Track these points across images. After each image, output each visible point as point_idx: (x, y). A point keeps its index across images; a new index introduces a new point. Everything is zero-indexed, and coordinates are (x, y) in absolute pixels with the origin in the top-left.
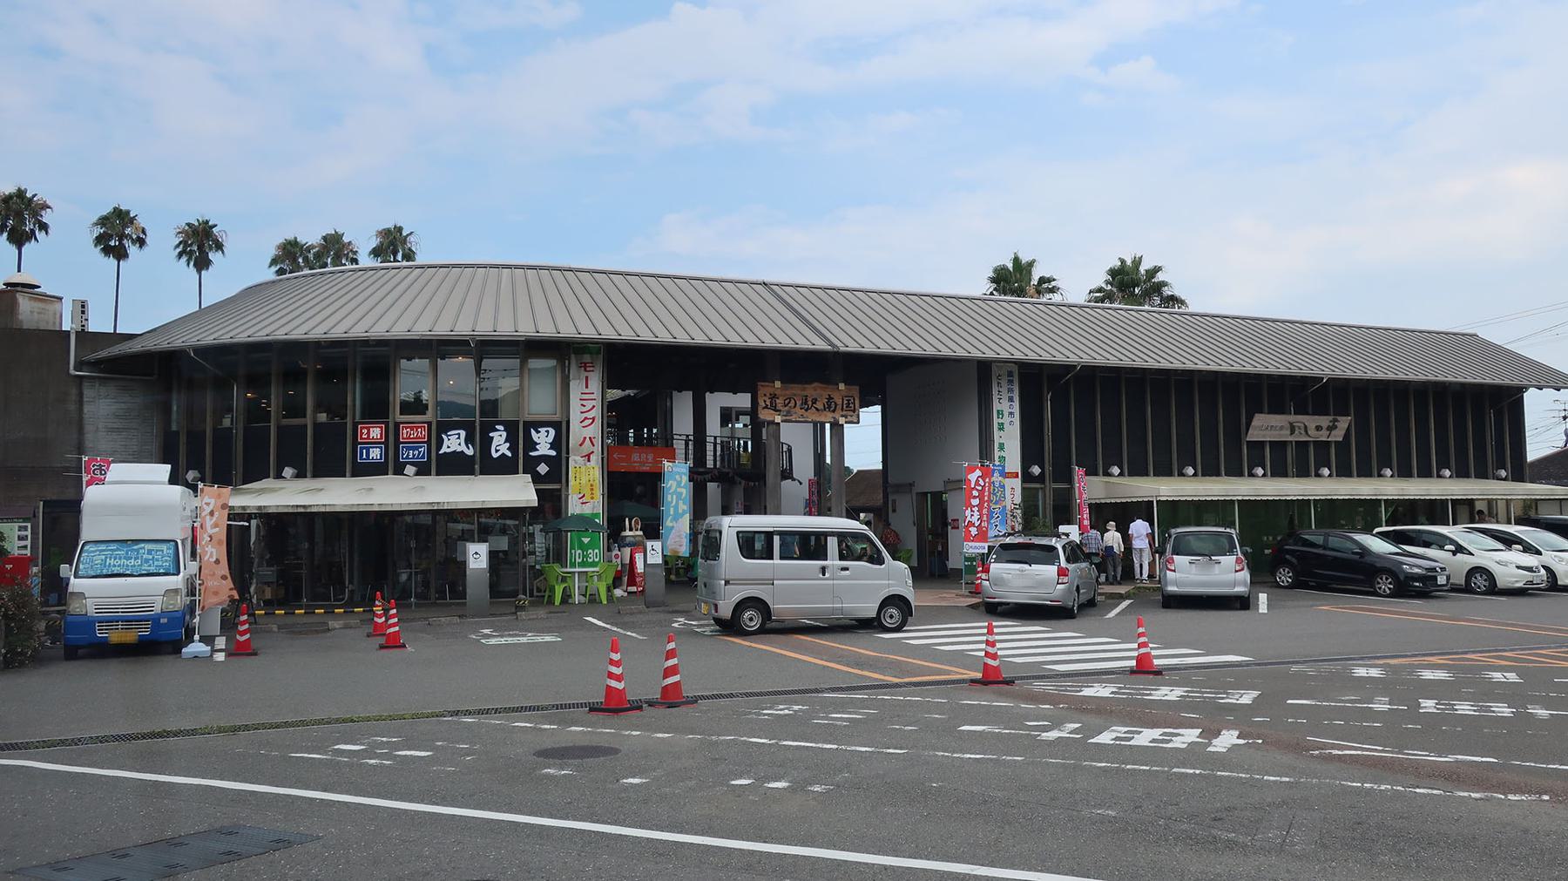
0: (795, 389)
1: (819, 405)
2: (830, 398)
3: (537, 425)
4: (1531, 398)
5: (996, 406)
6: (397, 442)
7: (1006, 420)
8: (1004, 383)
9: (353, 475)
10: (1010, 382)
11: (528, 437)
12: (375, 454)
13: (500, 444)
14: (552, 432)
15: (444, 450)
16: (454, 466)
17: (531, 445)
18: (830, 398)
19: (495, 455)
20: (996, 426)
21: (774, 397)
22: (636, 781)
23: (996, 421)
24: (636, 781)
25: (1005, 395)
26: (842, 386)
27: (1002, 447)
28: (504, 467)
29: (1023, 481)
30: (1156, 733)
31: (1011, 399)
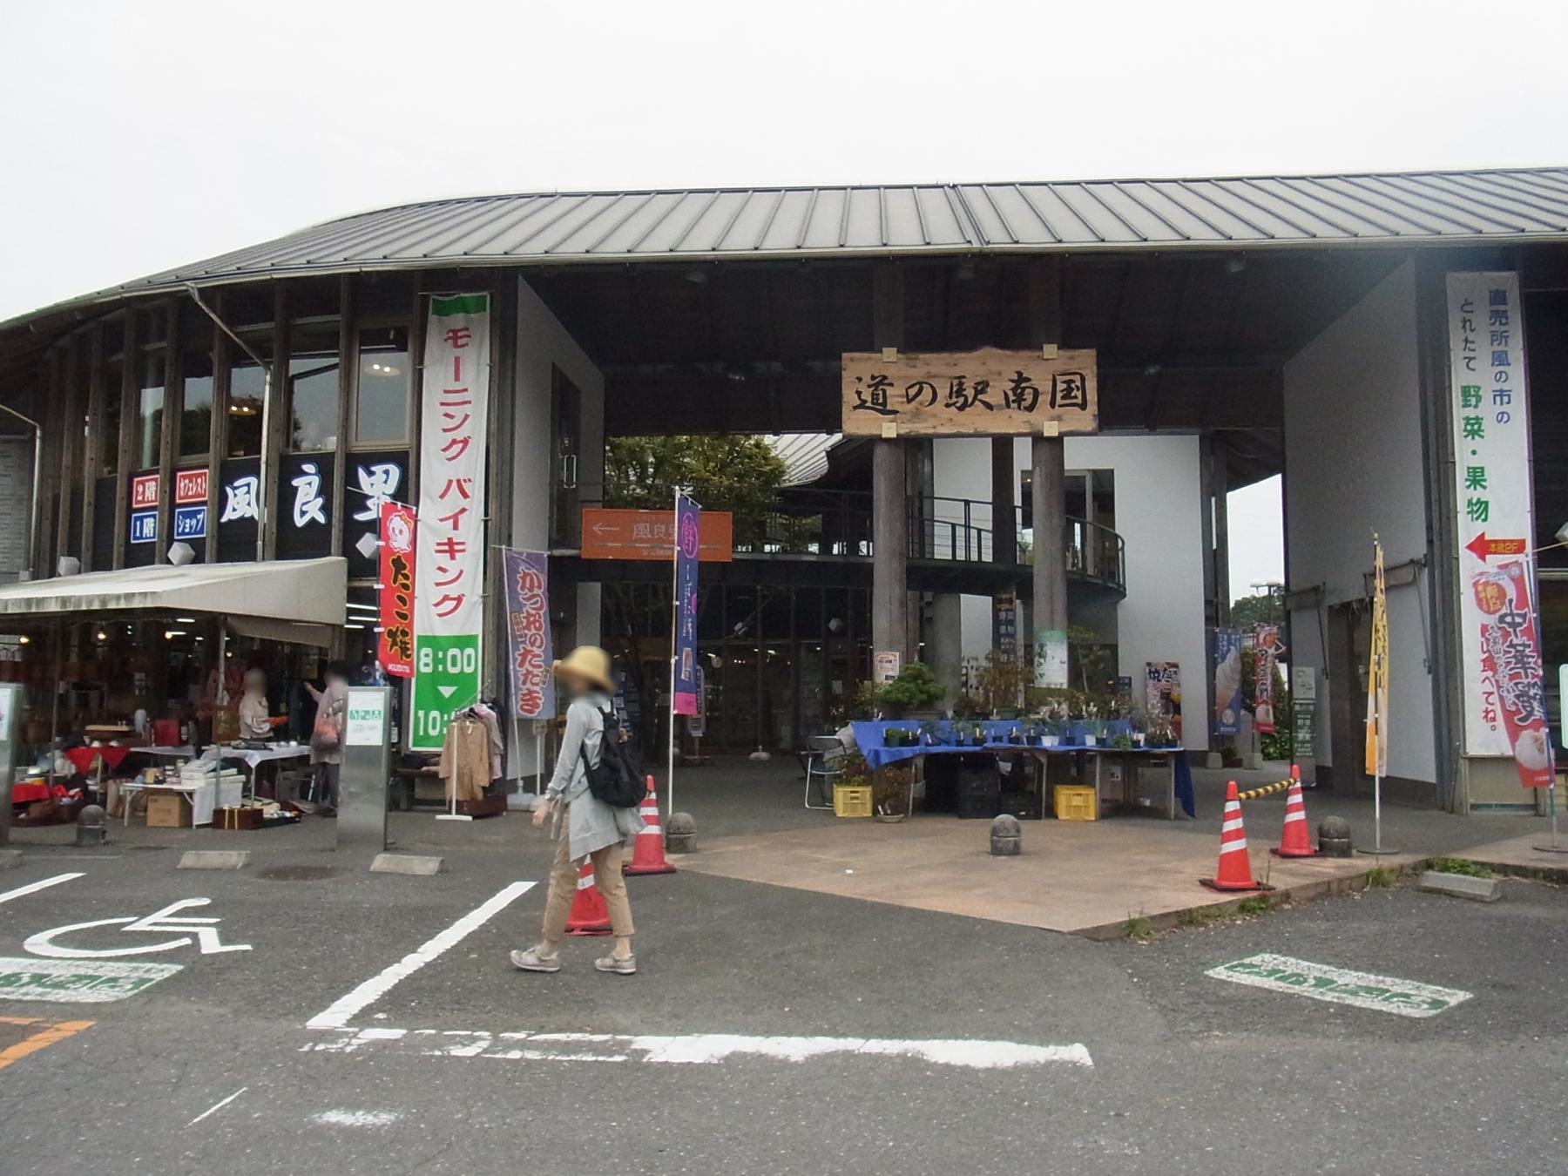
0: (938, 366)
1: (994, 396)
2: (1021, 379)
3: (370, 460)
4: (405, 357)
5: (1460, 377)
6: (173, 505)
7: (1487, 410)
8: (1481, 319)
9: (127, 565)
10: (1499, 316)
11: (351, 479)
12: (149, 528)
13: (308, 504)
14: (395, 471)
15: (224, 520)
16: (234, 543)
17: (357, 501)
18: (1021, 379)
19: (300, 522)
20: (1458, 426)
21: (880, 382)
22: (360, 1118)
23: (1459, 414)
24: (360, 1118)
25: (1484, 352)
26: (1050, 350)
27: (1476, 477)
28: (294, 542)
29: (1542, 560)
30: (485, 1038)
31: (1500, 359)
